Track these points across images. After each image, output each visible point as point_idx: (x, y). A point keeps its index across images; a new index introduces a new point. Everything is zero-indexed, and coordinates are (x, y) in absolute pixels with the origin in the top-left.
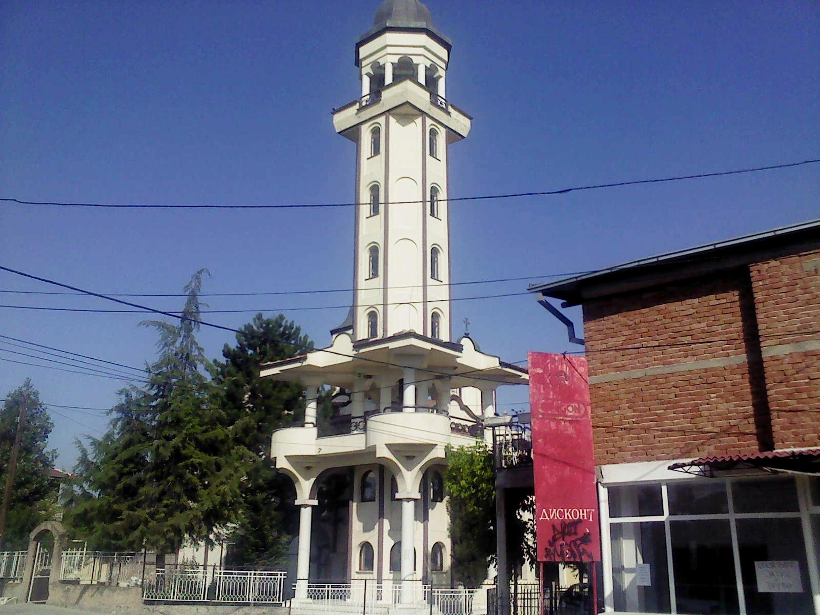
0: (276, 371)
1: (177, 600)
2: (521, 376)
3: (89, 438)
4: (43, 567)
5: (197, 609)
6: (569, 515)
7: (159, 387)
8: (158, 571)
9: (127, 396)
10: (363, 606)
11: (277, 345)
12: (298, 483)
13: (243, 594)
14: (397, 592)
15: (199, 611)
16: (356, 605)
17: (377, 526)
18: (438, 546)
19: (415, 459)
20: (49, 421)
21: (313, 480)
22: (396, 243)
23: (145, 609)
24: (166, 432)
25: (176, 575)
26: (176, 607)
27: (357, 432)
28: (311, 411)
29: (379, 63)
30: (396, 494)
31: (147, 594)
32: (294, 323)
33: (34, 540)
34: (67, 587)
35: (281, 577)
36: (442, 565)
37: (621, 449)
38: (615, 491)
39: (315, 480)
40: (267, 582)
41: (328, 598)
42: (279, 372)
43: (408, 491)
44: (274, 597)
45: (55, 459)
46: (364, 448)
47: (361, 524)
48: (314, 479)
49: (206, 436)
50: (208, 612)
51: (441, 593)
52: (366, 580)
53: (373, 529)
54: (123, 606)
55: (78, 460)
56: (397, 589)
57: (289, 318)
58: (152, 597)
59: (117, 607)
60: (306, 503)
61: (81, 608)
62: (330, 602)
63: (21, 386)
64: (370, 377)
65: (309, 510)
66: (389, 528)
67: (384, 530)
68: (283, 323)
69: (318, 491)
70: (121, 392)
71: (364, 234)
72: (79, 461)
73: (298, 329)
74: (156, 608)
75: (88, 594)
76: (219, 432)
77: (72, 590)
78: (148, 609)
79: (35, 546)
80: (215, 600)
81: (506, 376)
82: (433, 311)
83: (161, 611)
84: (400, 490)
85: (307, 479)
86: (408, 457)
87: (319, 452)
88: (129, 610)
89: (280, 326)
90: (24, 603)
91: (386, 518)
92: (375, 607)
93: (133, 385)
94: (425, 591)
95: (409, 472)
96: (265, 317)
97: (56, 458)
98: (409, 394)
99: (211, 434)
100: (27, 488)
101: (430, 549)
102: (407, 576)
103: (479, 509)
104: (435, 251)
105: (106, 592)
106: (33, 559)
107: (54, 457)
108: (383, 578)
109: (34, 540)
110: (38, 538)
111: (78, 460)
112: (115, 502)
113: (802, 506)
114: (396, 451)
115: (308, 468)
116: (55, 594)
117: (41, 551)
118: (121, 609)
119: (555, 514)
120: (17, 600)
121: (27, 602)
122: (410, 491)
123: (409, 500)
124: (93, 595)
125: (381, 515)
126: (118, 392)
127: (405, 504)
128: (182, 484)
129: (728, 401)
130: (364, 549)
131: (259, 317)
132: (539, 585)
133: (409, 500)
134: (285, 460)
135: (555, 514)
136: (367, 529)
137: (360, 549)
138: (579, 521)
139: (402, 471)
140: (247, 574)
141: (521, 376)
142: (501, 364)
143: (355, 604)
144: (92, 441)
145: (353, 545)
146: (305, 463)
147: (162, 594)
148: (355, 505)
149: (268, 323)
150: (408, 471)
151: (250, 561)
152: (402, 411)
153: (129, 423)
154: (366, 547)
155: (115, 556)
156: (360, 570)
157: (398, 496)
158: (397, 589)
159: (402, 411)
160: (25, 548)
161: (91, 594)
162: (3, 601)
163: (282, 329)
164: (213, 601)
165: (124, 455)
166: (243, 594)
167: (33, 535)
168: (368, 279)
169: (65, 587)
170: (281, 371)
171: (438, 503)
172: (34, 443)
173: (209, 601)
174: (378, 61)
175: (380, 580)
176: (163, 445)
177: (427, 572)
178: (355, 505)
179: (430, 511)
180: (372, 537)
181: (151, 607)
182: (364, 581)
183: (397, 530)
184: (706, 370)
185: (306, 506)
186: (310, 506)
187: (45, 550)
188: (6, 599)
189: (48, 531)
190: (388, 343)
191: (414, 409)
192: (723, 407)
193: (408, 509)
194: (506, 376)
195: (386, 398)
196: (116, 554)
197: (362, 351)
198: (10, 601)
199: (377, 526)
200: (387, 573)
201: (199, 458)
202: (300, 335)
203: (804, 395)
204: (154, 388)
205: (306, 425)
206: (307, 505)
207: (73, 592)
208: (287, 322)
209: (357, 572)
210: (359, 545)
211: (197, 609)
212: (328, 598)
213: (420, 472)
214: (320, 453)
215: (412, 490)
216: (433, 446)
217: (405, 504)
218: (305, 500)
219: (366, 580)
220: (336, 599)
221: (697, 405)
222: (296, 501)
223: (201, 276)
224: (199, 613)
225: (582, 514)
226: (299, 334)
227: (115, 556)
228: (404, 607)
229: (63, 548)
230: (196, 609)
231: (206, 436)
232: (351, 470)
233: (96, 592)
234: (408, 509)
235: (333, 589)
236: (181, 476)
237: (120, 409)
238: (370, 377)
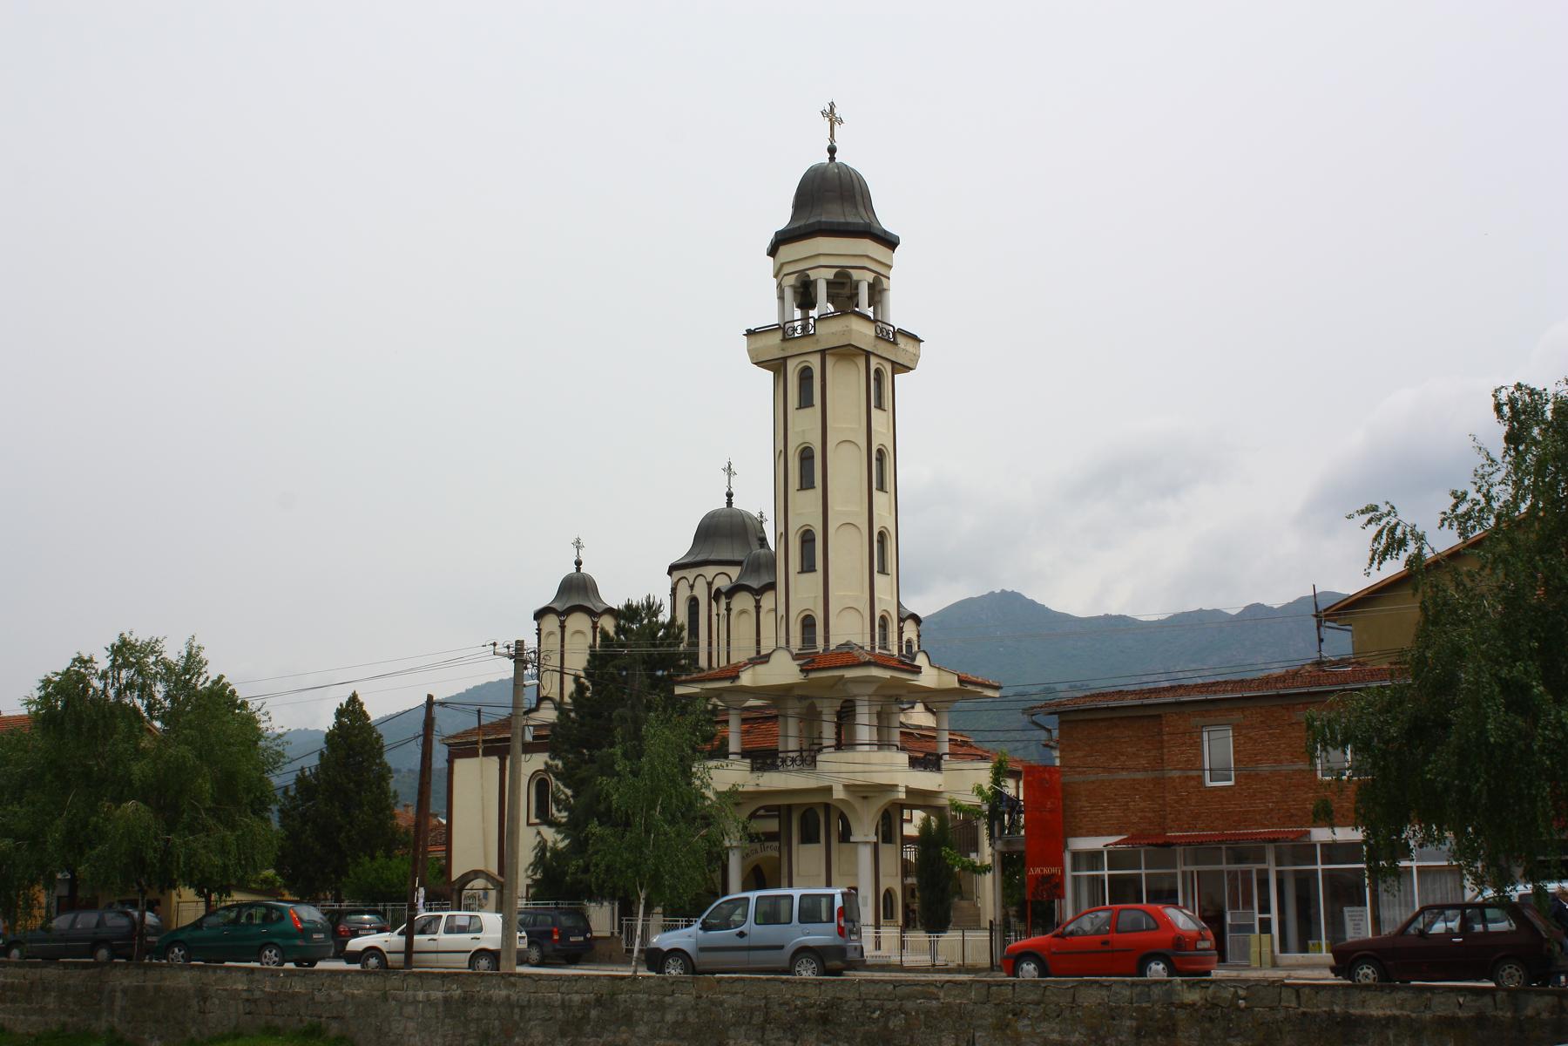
6: (1046, 871)
8: (664, 921)
18: (889, 892)
29: (808, 276)
37: (1080, 828)
38: (1076, 855)
55: (43, 682)
86: (865, 798)
103: (620, 743)
113: (1178, 866)
119: (1038, 870)
129: (1145, 801)
132: (934, 969)
135: (1038, 870)
138: (1052, 875)
142: (961, 681)
146: (734, 797)
174: (808, 272)
184: (1134, 780)
192: (1142, 805)
197: (813, 675)
203: (1184, 802)
221: (1128, 802)
225: (1054, 870)
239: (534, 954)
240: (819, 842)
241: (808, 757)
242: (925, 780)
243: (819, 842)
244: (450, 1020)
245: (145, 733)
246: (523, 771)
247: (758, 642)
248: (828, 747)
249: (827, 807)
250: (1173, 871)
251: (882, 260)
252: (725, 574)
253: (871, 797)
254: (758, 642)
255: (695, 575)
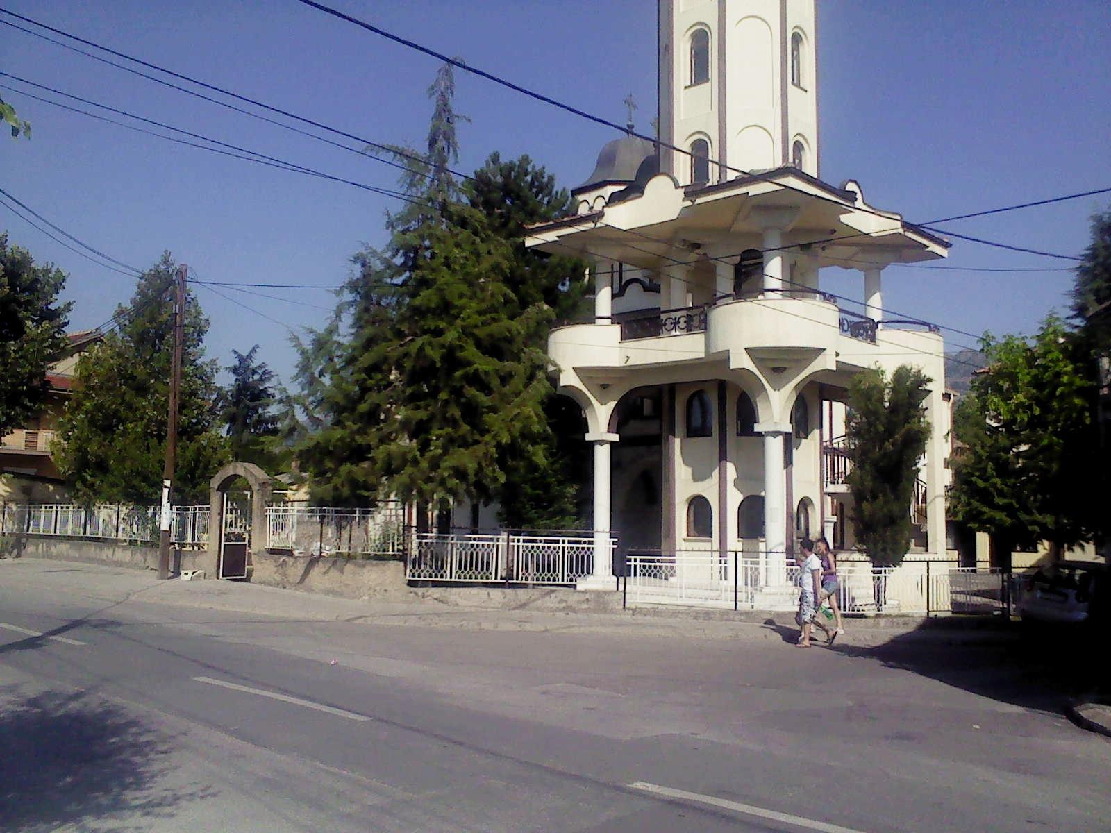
0: (551, 236)
1: (457, 580)
2: (928, 247)
3: (310, 333)
4: (233, 529)
5: (488, 594)
7: (405, 255)
9: (363, 265)
10: (734, 590)
11: (525, 203)
12: (764, 393)
13: (554, 572)
14: (749, 569)
15: (491, 597)
16: (678, 586)
17: (716, 473)
18: (805, 503)
19: (785, 372)
20: (200, 317)
21: (612, 404)
22: (737, 24)
23: (411, 592)
24: (431, 324)
25: (452, 544)
26: (455, 590)
27: (678, 333)
28: (604, 301)
30: (755, 425)
31: (411, 571)
32: (545, 170)
33: (217, 490)
34: (282, 559)
35: (564, 545)
36: (807, 529)
39: (617, 404)
40: (543, 552)
41: (635, 575)
42: (557, 239)
43: (775, 421)
44: (554, 575)
45: (215, 374)
46: (702, 355)
47: (689, 470)
48: (614, 403)
49: (488, 330)
50: (504, 598)
51: (751, 564)
52: (928, 562)
53: (710, 475)
54: (377, 588)
55: (297, 367)
56: (723, 565)
57: (536, 164)
58: (419, 576)
59: (369, 589)
60: (604, 439)
61: (310, 590)
62: (647, 582)
63: (158, 263)
64: (698, 246)
65: (607, 447)
66: (735, 476)
67: (728, 479)
68: (530, 169)
69: (620, 419)
70: (356, 259)
71: (682, 9)
72: (298, 369)
73: (551, 179)
74: (427, 591)
75: (317, 570)
76: (505, 324)
77: (291, 564)
78: (416, 593)
79: (220, 500)
80: (513, 580)
81: (908, 247)
82: (795, 140)
83: (435, 596)
84: (761, 419)
85: (603, 403)
86: (777, 370)
87: (626, 363)
88: (388, 594)
89: (526, 174)
90: (216, 579)
91: (731, 462)
92: (685, 588)
93: (371, 248)
94: (721, 568)
95: (604, 406)
96: (504, 160)
97: (217, 372)
98: (774, 268)
99: (494, 328)
100: (186, 416)
101: (795, 508)
102: (775, 546)
104: (797, 39)
105: (349, 567)
106: (219, 517)
107: (214, 370)
108: (1012, 566)
109: (217, 490)
110: (223, 487)
111: (297, 367)
112: (359, 432)
114: (762, 360)
115: (604, 386)
116: (262, 569)
117: (230, 507)
118: (376, 593)
120: (205, 574)
121: (218, 578)
122: (778, 421)
123: (775, 434)
124: (326, 572)
125: (723, 457)
126: (352, 259)
127: (769, 440)
128: (458, 404)
130: (692, 507)
131: (495, 158)
133: (775, 434)
134: (746, 357)
136: (697, 478)
137: (687, 505)
139: (768, 390)
140: (558, 542)
141: (928, 247)
143: (676, 584)
144: (314, 337)
145: (677, 501)
146: (600, 378)
147: (428, 571)
148: (677, 441)
149: (511, 167)
150: (602, 405)
151: (530, 521)
152: (594, 323)
153: (367, 310)
154: (699, 506)
155: (357, 515)
156: (688, 536)
157: (757, 428)
158: (723, 565)
159: (594, 323)
160: (204, 500)
161: (324, 570)
162: (186, 576)
163: (529, 178)
164: (510, 581)
165: (366, 360)
166: (554, 572)
167: (215, 483)
168: (689, 87)
169: (279, 559)
170: (558, 237)
171: (804, 441)
172: (186, 348)
173: (504, 581)
175: (723, 552)
176: (430, 344)
177: (792, 541)
178: (677, 441)
179: (794, 450)
180: (709, 490)
181: (420, 591)
182: (734, 554)
183: (753, 475)
185: (602, 442)
186: (606, 442)
187: (234, 504)
188: (190, 573)
189: (236, 476)
190: (747, 186)
191: (610, 320)
193: (774, 447)
194: (908, 247)
195: (725, 283)
196: (357, 512)
198: (196, 576)
199: (716, 473)
200: (734, 542)
201: (484, 364)
202: (555, 189)
204: (399, 255)
205: (598, 321)
206: (605, 441)
207: (293, 566)
208: (534, 167)
209: (684, 540)
210: (687, 500)
211: (488, 594)
212: (635, 575)
213: (794, 392)
214: (628, 364)
215: (781, 419)
216: (819, 351)
217: (769, 440)
218: (602, 434)
219: (928, 562)
220: (647, 577)
222: (587, 435)
223: (452, 70)
224: (491, 599)
226: (553, 187)
227: (357, 515)
228: (773, 591)
229: (266, 502)
230: (486, 592)
231: (488, 330)
232: (672, 388)
233: (330, 568)
234: (774, 447)
235: (642, 564)
236: (457, 392)
237: (353, 286)
238: (698, 246)
239: (226, 533)
240: (710, 435)
241: (697, 320)
242: (857, 353)
243: (710, 435)
244: (617, 607)
245: (499, 179)
246: (749, 187)
247: (731, 169)
248: (773, 290)
249: (722, 386)
250: (227, 543)
251: (657, 38)
252: (602, 196)
253: (790, 368)
254: (731, 169)
255: (597, 195)
